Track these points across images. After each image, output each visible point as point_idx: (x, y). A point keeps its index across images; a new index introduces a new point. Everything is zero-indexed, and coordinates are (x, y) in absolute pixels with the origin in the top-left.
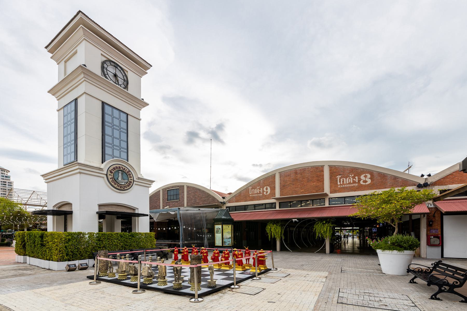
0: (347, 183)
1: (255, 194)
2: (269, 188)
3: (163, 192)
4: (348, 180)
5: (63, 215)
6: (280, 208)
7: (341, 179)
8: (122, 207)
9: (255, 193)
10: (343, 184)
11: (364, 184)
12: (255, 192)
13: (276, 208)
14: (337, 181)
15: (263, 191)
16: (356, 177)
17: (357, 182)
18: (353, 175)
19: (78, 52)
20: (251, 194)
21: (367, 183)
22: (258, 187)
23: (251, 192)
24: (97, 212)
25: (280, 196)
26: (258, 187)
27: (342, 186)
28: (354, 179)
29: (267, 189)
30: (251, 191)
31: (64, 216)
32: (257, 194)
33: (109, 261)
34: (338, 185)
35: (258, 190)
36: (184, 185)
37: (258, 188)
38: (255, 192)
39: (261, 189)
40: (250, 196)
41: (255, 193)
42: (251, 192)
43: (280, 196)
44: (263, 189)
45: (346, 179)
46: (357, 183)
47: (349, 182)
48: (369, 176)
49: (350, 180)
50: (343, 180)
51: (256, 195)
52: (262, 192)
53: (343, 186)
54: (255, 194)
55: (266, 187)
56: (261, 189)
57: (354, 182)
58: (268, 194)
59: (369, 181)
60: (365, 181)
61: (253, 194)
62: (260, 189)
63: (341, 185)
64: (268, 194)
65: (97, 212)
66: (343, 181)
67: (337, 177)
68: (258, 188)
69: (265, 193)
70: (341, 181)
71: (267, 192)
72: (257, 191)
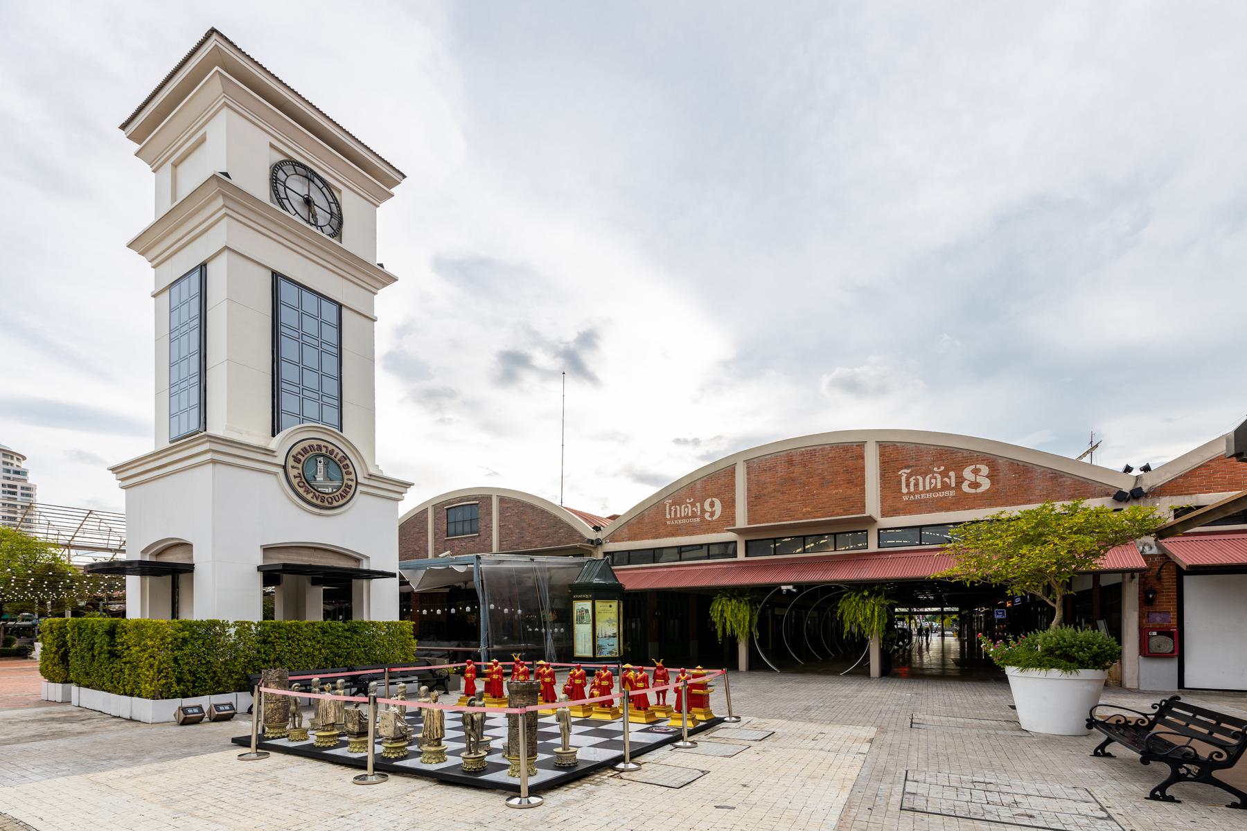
0: (928, 488)
1: (681, 518)
2: (717, 502)
3: (435, 514)
4: (930, 480)
6: (746, 556)
7: (911, 479)
8: (327, 554)
9: (681, 515)
10: (917, 491)
11: (973, 491)
12: (681, 512)
13: (736, 557)
14: (900, 482)
15: (703, 511)
16: (952, 474)
17: (953, 485)
18: (942, 468)
20: (671, 519)
21: (979, 490)
22: (688, 500)
23: (670, 514)
24: (258, 567)
25: (747, 523)
26: (690, 500)
27: (915, 497)
28: (946, 479)
29: (712, 505)
30: (670, 510)
31: (170, 577)
32: (687, 517)
33: (292, 697)
34: (904, 494)
35: (690, 507)
36: (492, 495)
37: (689, 503)
38: (681, 512)
39: (698, 505)
40: (668, 523)
41: (681, 515)
42: (670, 514)
43: (748, 524)
44: (702, 506)
45: (924, 479)
46: (953, 489)
47: (933, 486)
48: (985, 470)
49: (933, 481)
50: (917, 480)
51: (684, 521)
52: (699, 513)
53: (917, 496)
54: (681, 518)
55: (710, 500)
56: (698, 505)
57: (946, 487)
58: (715, 517)
59: (986, 484)
60: (975, 485)
61: (675, 518)
62: (693, 505)
63: (909, 493)
64: (715, 517)
65: (258, 567)
66: (916, 485)
67: (900, 473)
68: (689, 503)
69: (707, 516)
70: (912, 485)
71: (712, 514)
72: (686, 509)
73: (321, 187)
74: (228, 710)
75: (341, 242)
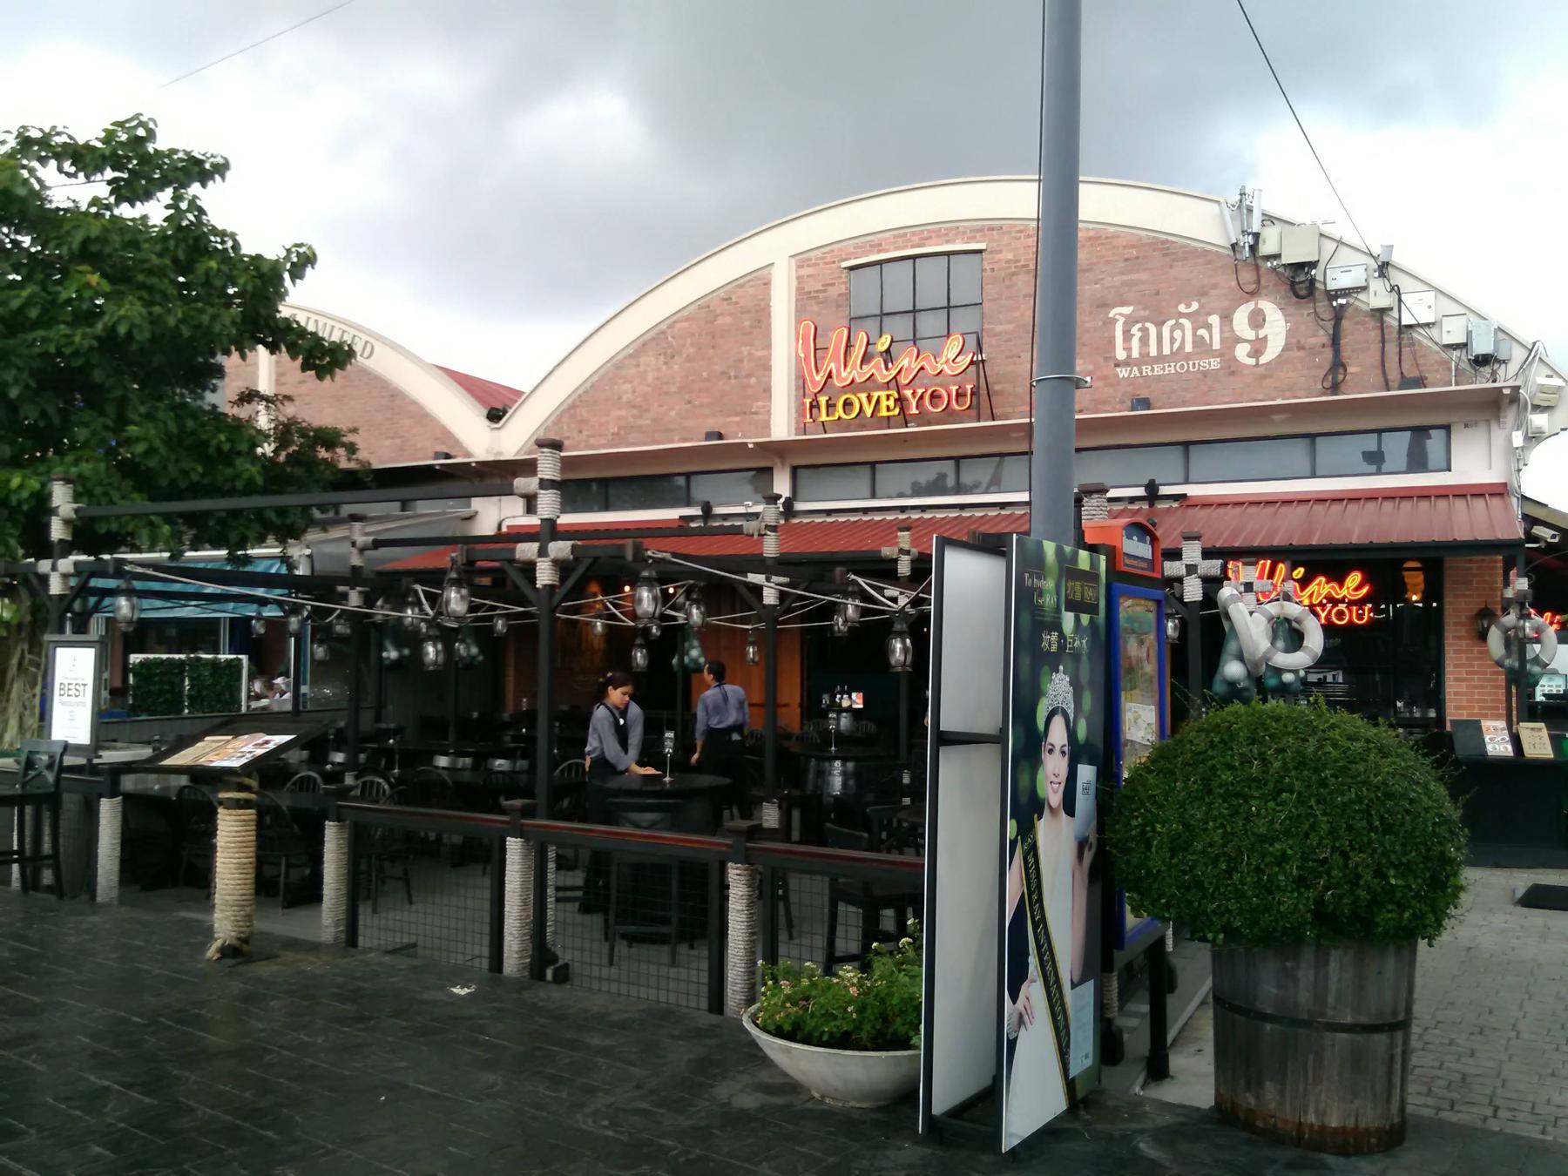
0: (1166, 351)
1: (1161, 358)
2: (1269, 307)
3: (805, 299)
5: (1112, 954)
15: (1231, 340)
17: (1216, 345)
18: (1195, 306)
19: (318, 253)
25: (793, 432)
26: (1188, 306)
27: (1153, 370)
29: (1257, 320)
30: (1127, 336)
32: (1177, 355)
37: (1187, 316)
39: (1214, 320)
41: (1128, 349)
42: (1128, 349)
43: (796, 435)
46: (1215, 354)
47: (1176, 346)
50: (1145, 330)
53: (1146, 370)
54: (1161, 358)
62: (1199, 320)
63: (1127, 363)
64: (1269, 356)
67: (1110, 315)
68: (1187, 316)
69: (1242, 352)
71: (1258, 348)
73: (841, 947)
74: (1142, 569)
75: (1074, 986)
